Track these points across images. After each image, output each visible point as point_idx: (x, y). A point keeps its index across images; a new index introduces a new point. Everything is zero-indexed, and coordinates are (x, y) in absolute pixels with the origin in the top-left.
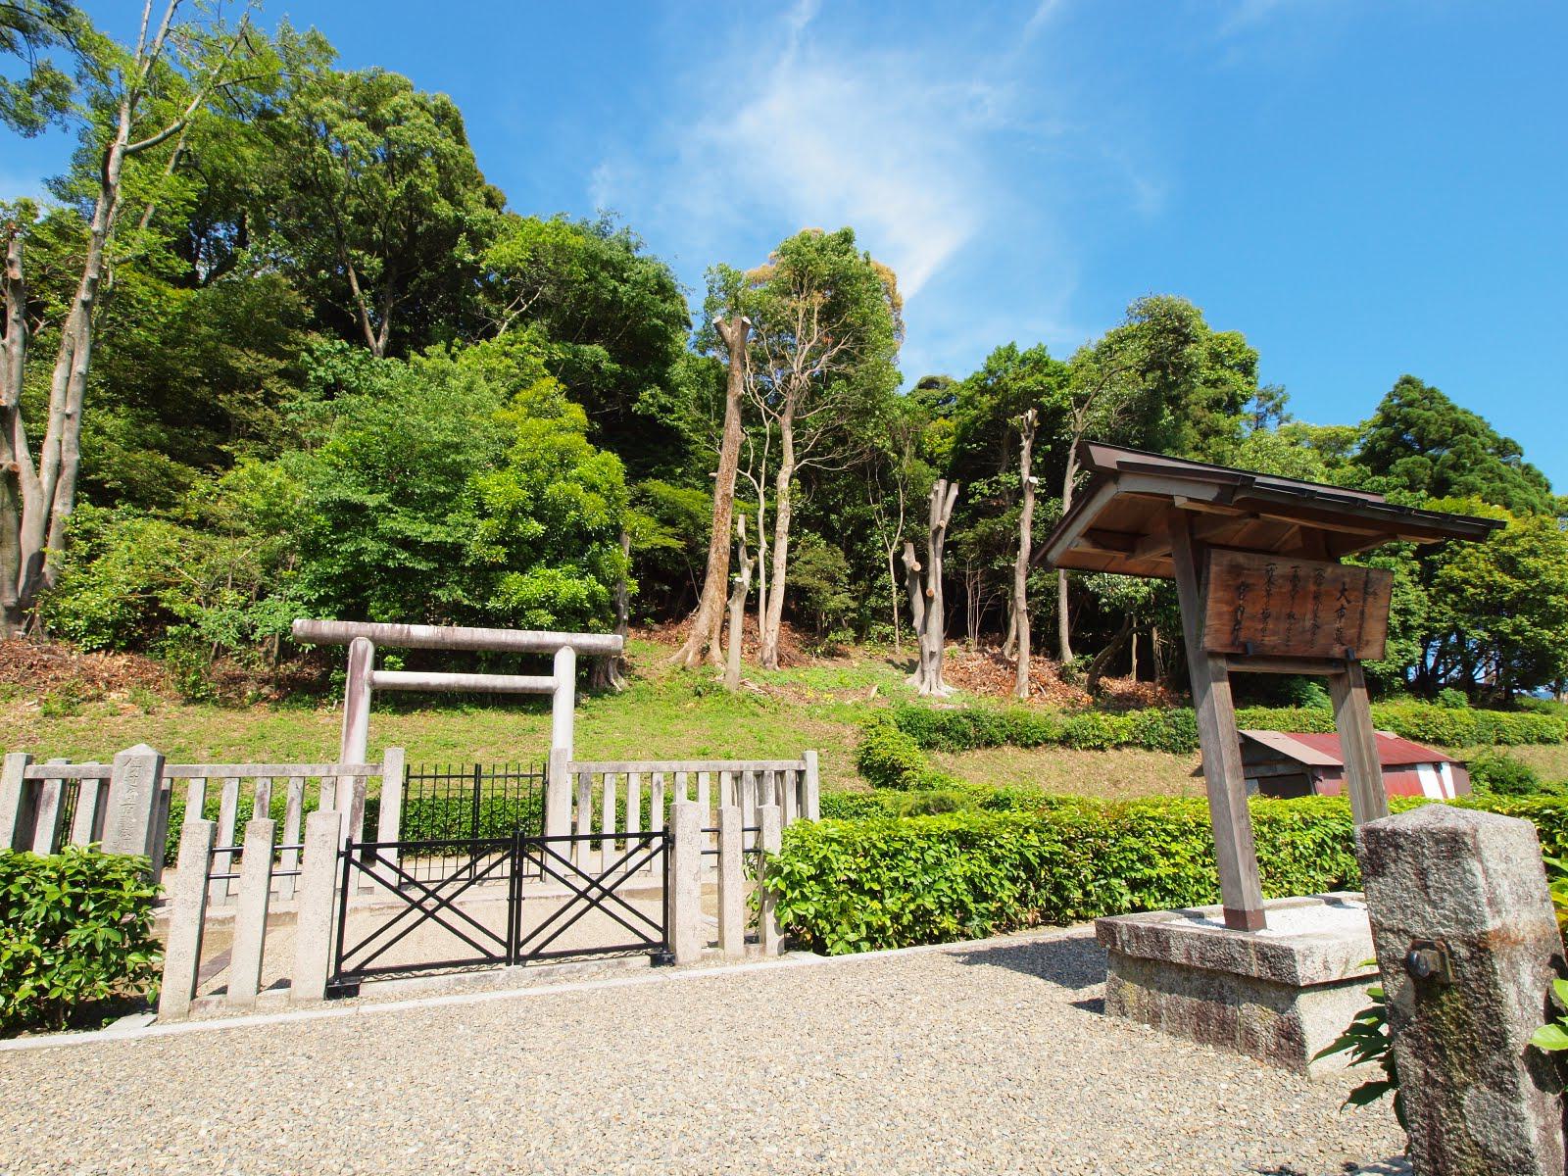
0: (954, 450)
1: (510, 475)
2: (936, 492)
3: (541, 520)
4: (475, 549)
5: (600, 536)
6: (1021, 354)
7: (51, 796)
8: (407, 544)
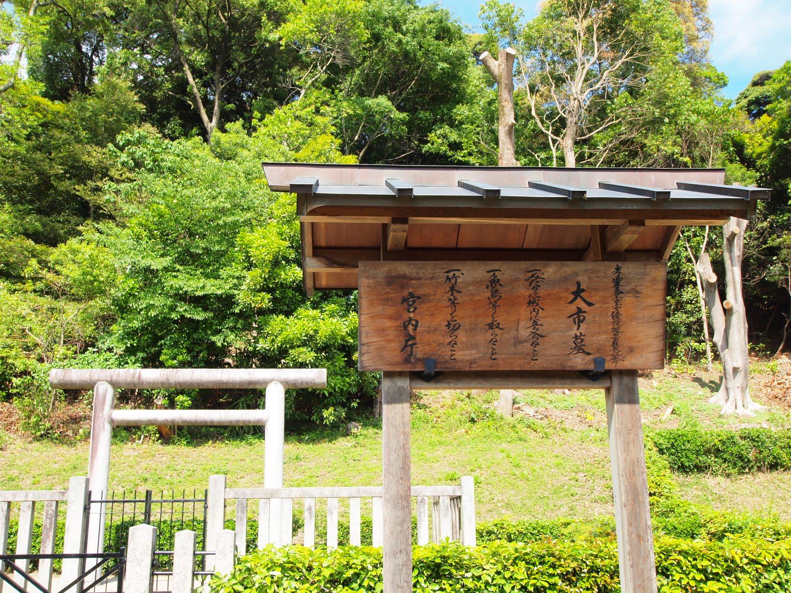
4: (243, 298)
8: (183, 297)
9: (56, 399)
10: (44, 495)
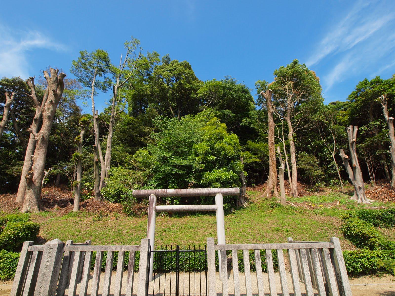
0: (349, 119)
1: (204, 144)
2: (349, 130)
3: (214, 155)
5: (233, 159)
6: (370, 81)
7: (34, 257)
8: (175, 166)
9: (134, 202)
10: (130, 248)
